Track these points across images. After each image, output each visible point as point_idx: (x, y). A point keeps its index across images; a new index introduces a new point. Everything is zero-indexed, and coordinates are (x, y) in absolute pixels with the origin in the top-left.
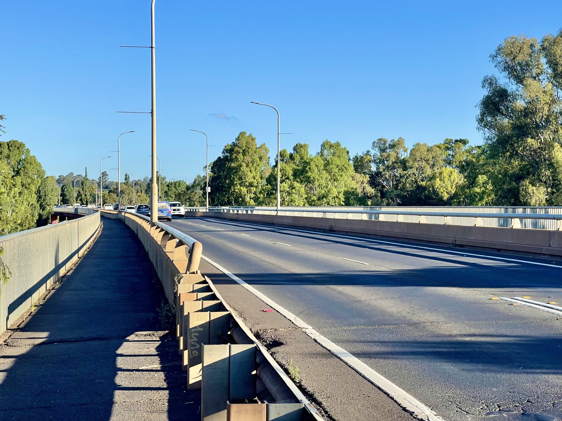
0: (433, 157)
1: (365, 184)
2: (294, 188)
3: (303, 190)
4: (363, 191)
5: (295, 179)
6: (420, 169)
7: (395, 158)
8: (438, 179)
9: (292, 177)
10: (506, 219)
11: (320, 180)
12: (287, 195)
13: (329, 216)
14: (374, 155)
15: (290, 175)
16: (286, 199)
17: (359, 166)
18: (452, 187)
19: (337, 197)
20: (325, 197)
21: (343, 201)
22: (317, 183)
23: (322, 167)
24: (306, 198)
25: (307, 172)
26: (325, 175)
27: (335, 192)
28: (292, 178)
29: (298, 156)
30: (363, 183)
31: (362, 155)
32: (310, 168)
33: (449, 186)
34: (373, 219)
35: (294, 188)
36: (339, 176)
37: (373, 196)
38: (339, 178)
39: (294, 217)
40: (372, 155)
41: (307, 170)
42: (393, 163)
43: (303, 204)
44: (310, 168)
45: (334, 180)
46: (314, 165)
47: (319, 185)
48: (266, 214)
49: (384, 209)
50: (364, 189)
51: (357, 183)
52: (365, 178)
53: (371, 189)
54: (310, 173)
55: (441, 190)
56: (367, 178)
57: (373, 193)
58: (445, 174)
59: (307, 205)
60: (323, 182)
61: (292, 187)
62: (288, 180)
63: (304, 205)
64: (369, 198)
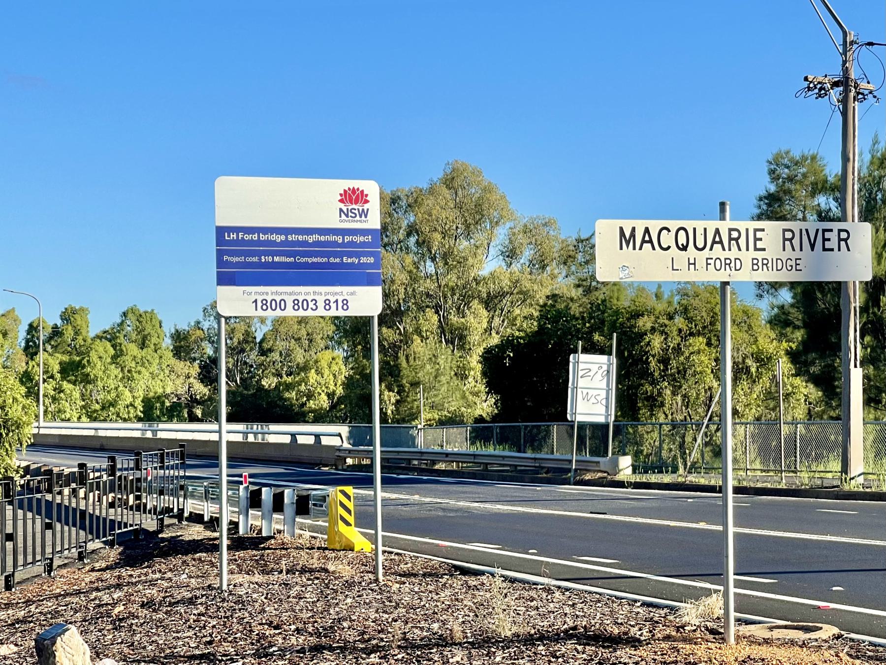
0: (308, 334)
1: (192, 380)
2: (62, 391)
3: (77, 395)
4: (189, 390)
5: (63, 378)
6: (287, 355)
7: (243, 335)
8: (313, 371)
9: (59, 375)
10: (246, 434)
11: (105, 378)
12: (50, 401)
13: (102, 433)
14: (208, 329)
15: (55, 371)
16: (50, 409)
17: (181, 347)
18: (336, 385)
19: (132, 405)
20: (113, 406)
21: (140, 411)
22: (100, 384)
23: (109, 360)
24: (83, 407)
25: (84, 367)
26: (114, 371)
27: (127, 397)
28: (58, 376)
29: (70, 328)
30: (189, 377)
31: (187, 328)
32: (88, 361)
33: (332, 382)
34: (260, 441)
35: (62, 391)
36: (136, 372)
37: (206, 401)
38: (136, 375)
39: (60, 435)
40: (205, 328)
41: (84, 364)
42: (239, 343)
43: (78, 415)
44: (88, 361)
45: (129, 379)
46: (96, 357)
47: (104, 387)
48: (62, 433)
49: (162, 426)
50: (190, 387)
51: (178, 376)
52: (192, 369)
53: (203, 388)
54: (89, 369)
55: (319, 389)
56: (195, 370)
57: (205, 395)
58: (324, 364)
59: (84, 418)
60: (112, 384)
61: (60, 390)
62: (51, 380)
63: (80, 418)
64: (199, 403)
